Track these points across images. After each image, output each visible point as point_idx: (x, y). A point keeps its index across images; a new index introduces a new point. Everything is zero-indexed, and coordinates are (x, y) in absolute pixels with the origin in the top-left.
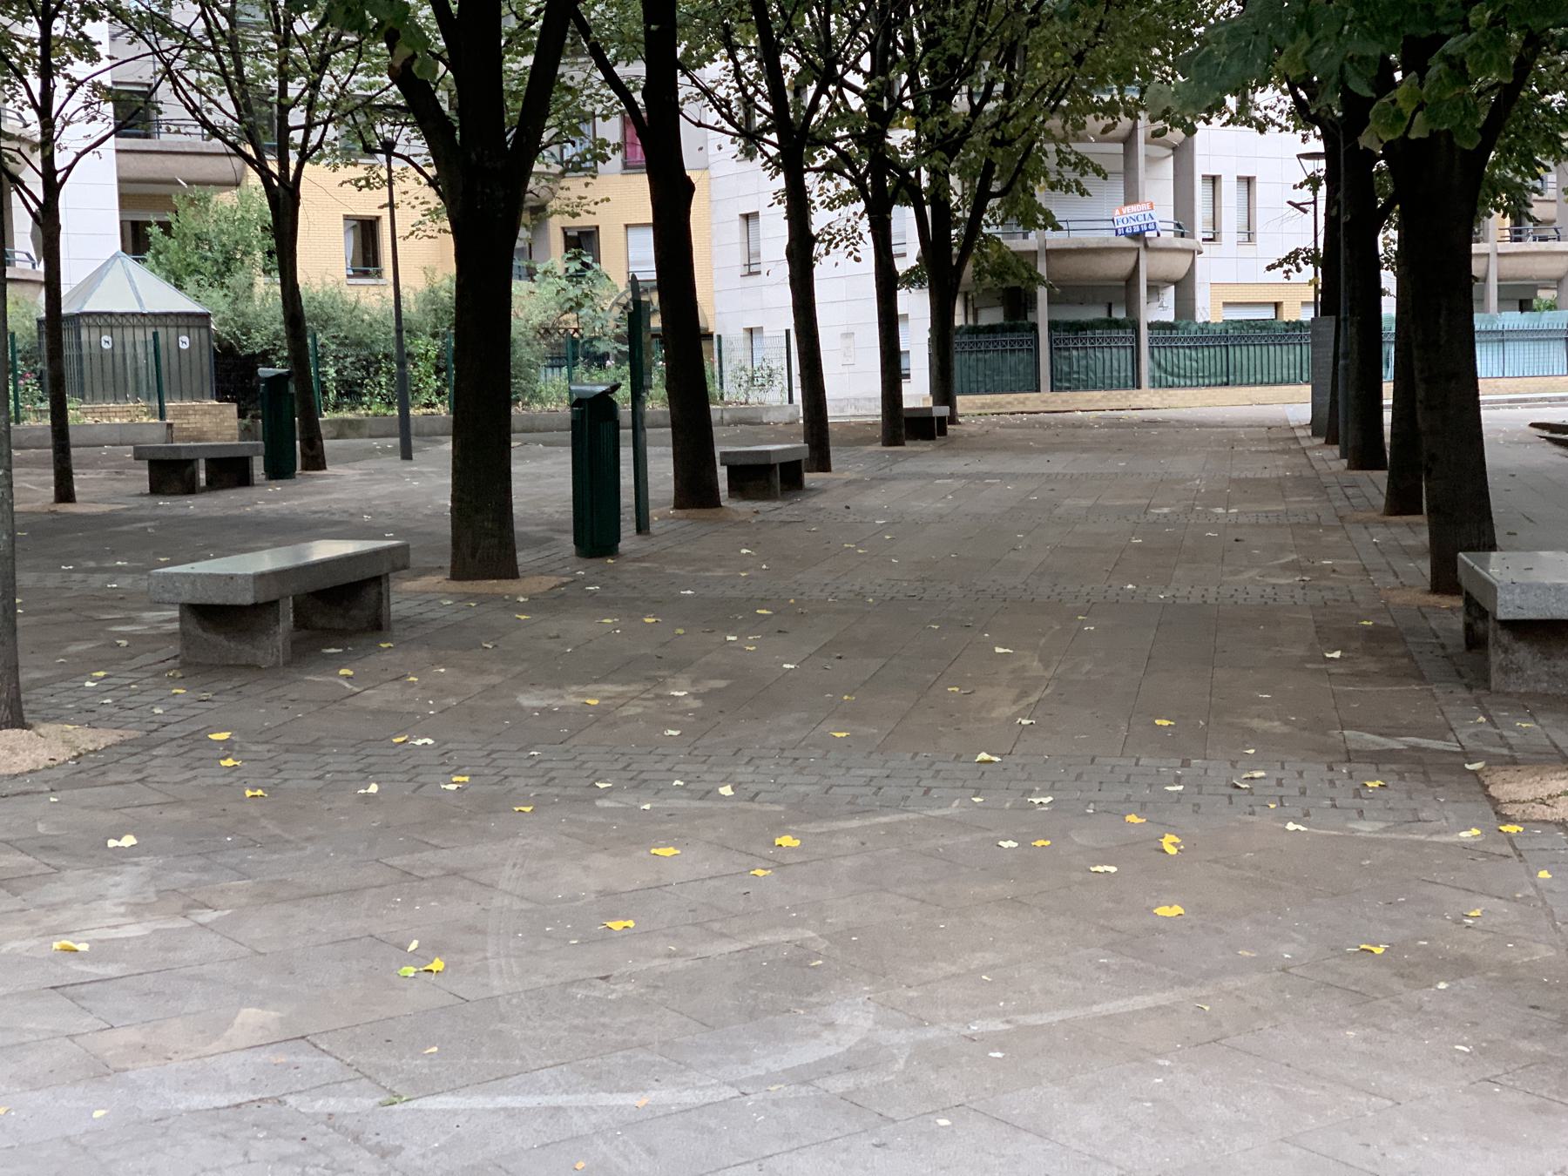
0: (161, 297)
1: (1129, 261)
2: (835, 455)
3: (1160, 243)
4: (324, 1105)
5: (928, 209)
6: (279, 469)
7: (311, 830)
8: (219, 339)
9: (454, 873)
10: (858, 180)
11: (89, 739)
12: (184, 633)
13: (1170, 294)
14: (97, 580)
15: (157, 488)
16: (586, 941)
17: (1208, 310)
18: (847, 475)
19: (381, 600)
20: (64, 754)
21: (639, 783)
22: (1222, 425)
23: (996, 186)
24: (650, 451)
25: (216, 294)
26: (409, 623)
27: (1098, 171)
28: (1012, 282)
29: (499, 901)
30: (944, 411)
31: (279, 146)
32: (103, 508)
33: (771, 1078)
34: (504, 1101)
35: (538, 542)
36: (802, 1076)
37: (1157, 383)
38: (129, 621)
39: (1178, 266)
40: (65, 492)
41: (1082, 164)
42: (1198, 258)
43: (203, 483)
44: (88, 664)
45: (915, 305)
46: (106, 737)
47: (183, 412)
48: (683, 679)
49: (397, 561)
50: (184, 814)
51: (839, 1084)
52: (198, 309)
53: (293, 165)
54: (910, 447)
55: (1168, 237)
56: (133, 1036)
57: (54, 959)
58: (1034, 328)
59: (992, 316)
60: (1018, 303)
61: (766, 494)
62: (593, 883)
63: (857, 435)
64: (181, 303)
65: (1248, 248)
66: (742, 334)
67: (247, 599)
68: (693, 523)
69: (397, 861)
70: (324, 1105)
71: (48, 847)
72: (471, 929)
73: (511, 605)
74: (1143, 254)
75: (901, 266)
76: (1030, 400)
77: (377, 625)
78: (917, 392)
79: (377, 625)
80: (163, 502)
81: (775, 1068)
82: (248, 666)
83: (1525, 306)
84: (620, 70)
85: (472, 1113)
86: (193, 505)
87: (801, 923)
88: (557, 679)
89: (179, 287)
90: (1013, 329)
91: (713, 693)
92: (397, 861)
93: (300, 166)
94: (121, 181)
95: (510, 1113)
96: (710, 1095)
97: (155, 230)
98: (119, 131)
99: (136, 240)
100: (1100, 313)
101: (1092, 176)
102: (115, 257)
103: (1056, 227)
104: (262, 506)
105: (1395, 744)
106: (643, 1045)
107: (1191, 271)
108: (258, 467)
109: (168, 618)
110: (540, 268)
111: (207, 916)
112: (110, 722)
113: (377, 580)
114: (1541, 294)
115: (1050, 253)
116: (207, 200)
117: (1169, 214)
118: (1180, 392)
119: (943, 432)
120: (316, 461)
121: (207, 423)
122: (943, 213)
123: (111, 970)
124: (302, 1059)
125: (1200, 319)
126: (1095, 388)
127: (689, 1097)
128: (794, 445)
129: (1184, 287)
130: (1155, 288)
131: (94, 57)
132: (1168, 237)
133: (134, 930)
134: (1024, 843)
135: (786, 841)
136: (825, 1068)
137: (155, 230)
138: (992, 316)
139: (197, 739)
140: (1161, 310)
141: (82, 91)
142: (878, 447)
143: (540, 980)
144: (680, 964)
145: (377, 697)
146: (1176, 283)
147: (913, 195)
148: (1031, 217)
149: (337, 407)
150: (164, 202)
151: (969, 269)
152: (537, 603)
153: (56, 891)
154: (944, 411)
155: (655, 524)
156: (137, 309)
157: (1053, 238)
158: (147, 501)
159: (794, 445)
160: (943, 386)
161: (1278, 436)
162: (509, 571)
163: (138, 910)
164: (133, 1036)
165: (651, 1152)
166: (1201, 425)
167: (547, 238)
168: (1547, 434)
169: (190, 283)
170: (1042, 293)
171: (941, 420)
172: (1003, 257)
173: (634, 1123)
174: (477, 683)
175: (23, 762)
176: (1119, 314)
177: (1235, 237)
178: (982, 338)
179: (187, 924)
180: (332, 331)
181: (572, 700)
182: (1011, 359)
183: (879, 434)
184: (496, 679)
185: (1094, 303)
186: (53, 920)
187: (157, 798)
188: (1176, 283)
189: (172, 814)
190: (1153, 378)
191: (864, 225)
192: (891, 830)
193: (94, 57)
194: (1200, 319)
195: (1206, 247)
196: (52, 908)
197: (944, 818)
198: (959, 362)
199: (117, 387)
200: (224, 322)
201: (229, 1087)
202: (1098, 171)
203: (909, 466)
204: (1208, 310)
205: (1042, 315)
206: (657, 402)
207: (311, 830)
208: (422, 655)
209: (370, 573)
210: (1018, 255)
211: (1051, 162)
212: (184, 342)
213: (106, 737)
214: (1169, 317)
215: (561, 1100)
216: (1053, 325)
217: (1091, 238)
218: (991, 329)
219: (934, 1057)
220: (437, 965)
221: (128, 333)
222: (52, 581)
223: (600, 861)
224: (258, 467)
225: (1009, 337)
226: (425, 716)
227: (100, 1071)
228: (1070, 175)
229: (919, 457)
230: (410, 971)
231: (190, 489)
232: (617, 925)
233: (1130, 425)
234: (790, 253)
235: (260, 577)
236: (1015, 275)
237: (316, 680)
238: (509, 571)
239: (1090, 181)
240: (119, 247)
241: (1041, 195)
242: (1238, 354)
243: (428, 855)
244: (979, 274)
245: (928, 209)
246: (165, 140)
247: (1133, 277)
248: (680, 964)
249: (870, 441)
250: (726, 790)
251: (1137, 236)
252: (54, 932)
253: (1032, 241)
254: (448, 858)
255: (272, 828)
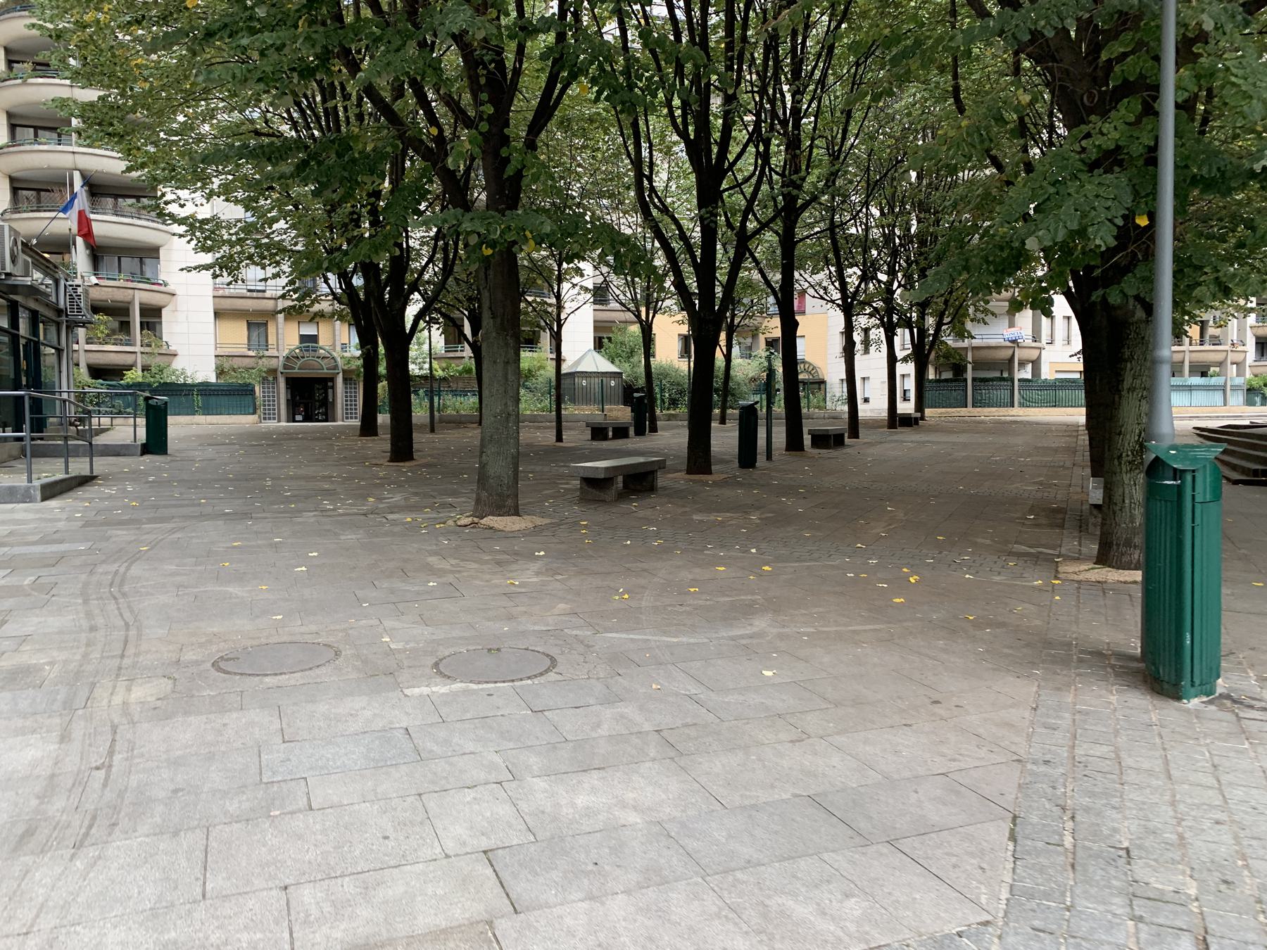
0: (605, 366)
1: (1010, 352)
2: (862, 432)
3: (1024, 344)
4: (575, 632)
5: (915, 330)
6: (640, 432)
7: (602, 554)
8: (626, 382)
9: (645, 570)
10: (881, 319)
11: (539, 521)
12: (581, 488)
13: (1029, 367)
14: (561, 470)
15: (593, 438)
16: (679, 594)
17: (1047, 373)
18: (866, 440)
19: (654, 480)
20: (530, 525)
21: (723, 547)
22: (1047, 424)
23: (946, 320)
24: (774, 429)
25: (627, 365)
26: (664, 488)
27: (993, 314)
28: (952, 361)
29: (656, 580)
30: (919, 415)
31: (519, 326)
32: (573, 445)
33: (723, 638)
34: (631, 636)
35: (722, 461)
36: (732, 639)
37: (1021, 405)
38: (567, 484)
39: (1033, 354)
40: (559, 438)
41: (986, 311)
42: (1043, 352)
43: (24, 383)
44: (547, 498)
45: (906, 369)
46: (547, 521)
47: (611, 410)
48: (758, 513)
49: (661, 465)
50: (562, 547)
51: (744, 642)
52: (618, 371)
53: (651, 315)
54: (900, 429)
55: (1029, 342)
56: (523, 609)
57: (507, 586)
58: (966, 380)
59: (947, 375)
60: (959, 370)
61: (827, 447)
62: (690, 577)
63: (874, 424)
64: (613, 369)
65: (1068, 347)
66: (838, 381)
67: (602, 476)
68: (793, 459)
69: (627, 566)
70: (575, 632)
71: (516, 554)
72: (643, 587)
73: (706, 484)
74: (1016, 349)
75: (900, 354)
76: (963, 411)
77: (652, 489)
78: (906, 407)
79: (652, 489)
80: (595, 443)
81: (725, 634)
82: (602, 501)
83: (1204, 374)
84: (770, 276)
85: (620, 638)
86: (604, 445)
87: (756, 594)
88: (709, 510)
89: (612, 362)
90: (955, 381)
91: (766, 518)
92: (627, 566)
93: (653, 317)
94: (595, 321)
95: (632, 639)
96: (700, 641)
97: (606, 340)
98: (595, 302)
99: (599, 344)
100: (998, 374)
101: (990, 316)
102: (589, 350)
103: (973, 338)
104: (630, 446)
105: (1032, 550)
106: (684, 625)
107: (1039, 357)
108: (632, 431)
109: (577, 483)
110: (753, 354)
111: (559, 577)
112: (549, 516)
113: (653, 472)
114: (1212, 369)
115: (973, 348)
116: (625, 329)
117: (1030, 332)
118: (1033, 409)
119: (917, 423)
120: (654, 429)
121: (619, 414)
122: (923, 332)
123: (523, 590)
124: (574, 620)
125: (1043, 377)
126: (993, 406)
127: (692, 640)
128: (842, 426)
129: (1036, 364)
130: (1022, 364)
131: (582, 275)
132: (1029, 342)
133: (535, 580)
134: (857, 575)
135: (766, 568)
136: (742, 637)
137: (606, 340)
138: (947, 375)
139: (576, 523)
140: (1027, 373)
141: (577, 288)
142: (886, 430)
143: (658, 604)
144: (708, 603)
145: (641, 514)
146: (1032, 362)
147: (908, 324)
148: (961, 334)
149: (668, 409)
150: (609, 329)
151: (933, 355)
152: (715, 484)
153: (514, 567)
154: (919, 415)
155: (775, 454)
156: (595, 370)
157: (975, 342)
158: (589, 443)
159: (842, 426)
160: (920, 406)
161: (1070, 429)
162: (708, 471)
163: (537, 574)
164: (523, 609)
165: (672, 654)
166: (1037, 423)
167: (758, 343)
168: (1198, 432)
169: (617, 361)
170: (969, 367)
171: (916, 419)
172: (948, 350)
173: (669, 646)
174: (680, 510)
175: (516, 527)
176: (1006, 375)
177: (1062, 342)
178: (942, 384)
179: (550, 579)
180: (668, 379)
181: (712, 518)
182: (954, 394)
183: (886, 423)
184: (688, 509)
185: (995, 369)
186: (511, 575)
187: (556, 541)
188: (1032, 362)
189: (559, 546)
190: (1020, 403)
191: (883, 338)
192: (808, 567)
193: (582, 275)
194: (1043, 377)
195: (1047, 347)
196: (511, 571)
197: (833, 566)
198: (928, 395)
199: (586, 398)
200: (628, 376)
201: (548, 625)
202: (993, 314)
203: (895, 437)
204: (1047, 373)
205: (969, 375)
206: (779, 408)
207: (602, 554)
208: (666, 500)
209: (649, 469)
210: (956, 349)
211: (971, 310)
212: (613, 384)
213: (547, 521)
214: (1029, 376)
215: (650, 638)
216: (974, 379)
217: (993, 342)
218: (946, 380)
219: (781, 637)
220: (626, 596)
221: (592, 380)
222: (546, 469)
223: (697, 570)
224: (632, 431)
225: (954, 384)
226: (657, 520)
227: (511, 618)
228: (979, 315)
229: (907, 436)
230: (617, 598)
231: (605, 438)
232: (692, 590)
233: (1005, 423)
234: (845, 349)
235: (607, 469)
236: (954, 358)
237: (624, 506)
238: (708, 471)
239: (988, 318)
240: (590, 344)
241: (969, 325)
242: (1061, 393)
243: (639, 565)
244: (938, 357)
245: (915, 330)
246: (609, 307)
247: (1011, 359)
248: (708, 603)
249: (882, 427)
250: (754, 551)
251: (1014, 341)
252: (509, 579)
253: (966, 343)
254: (645, 566)
255: (591, 553)
